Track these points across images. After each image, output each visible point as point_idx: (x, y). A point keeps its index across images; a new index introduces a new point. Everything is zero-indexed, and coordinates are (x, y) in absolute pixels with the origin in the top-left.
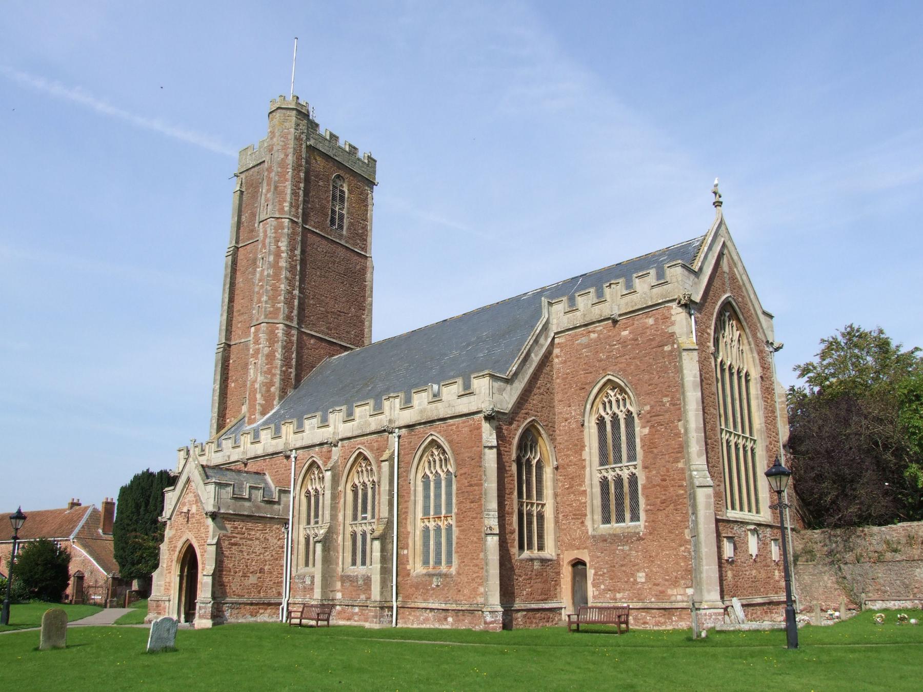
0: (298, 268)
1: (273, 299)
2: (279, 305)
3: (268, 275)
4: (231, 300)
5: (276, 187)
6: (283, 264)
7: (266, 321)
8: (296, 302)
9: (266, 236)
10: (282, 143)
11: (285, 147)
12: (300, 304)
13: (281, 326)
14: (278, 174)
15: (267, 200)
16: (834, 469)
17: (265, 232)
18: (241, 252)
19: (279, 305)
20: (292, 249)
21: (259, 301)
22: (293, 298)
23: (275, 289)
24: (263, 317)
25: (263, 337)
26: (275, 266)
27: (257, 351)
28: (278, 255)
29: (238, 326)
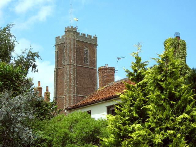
0: (76, 78)
1: (70, 88)
2: (71, 90)
3: (68, 81)
4: (57, 85)
5: (68, 55)
6: (72, 78)
7: (68, 94)
8: (76, 88)
9: (66, 70)
10: (70, 42)
11: (70, 43)
12: (77, 88)
13: (72, 96)
14: (69, 51)
15: (66, 59)
16: (147, 124)
17: (66, 68)
18: (59, 70)
19: (71, 90)
20: (74, 73)
21: (66, 88)
22: (75, 87)
23: (70, 85)
24: (67, 93)
25: (67, 99)
26: (70, 79)
27: (66, 103)
28: (70, 75)
29: (59, 92)
